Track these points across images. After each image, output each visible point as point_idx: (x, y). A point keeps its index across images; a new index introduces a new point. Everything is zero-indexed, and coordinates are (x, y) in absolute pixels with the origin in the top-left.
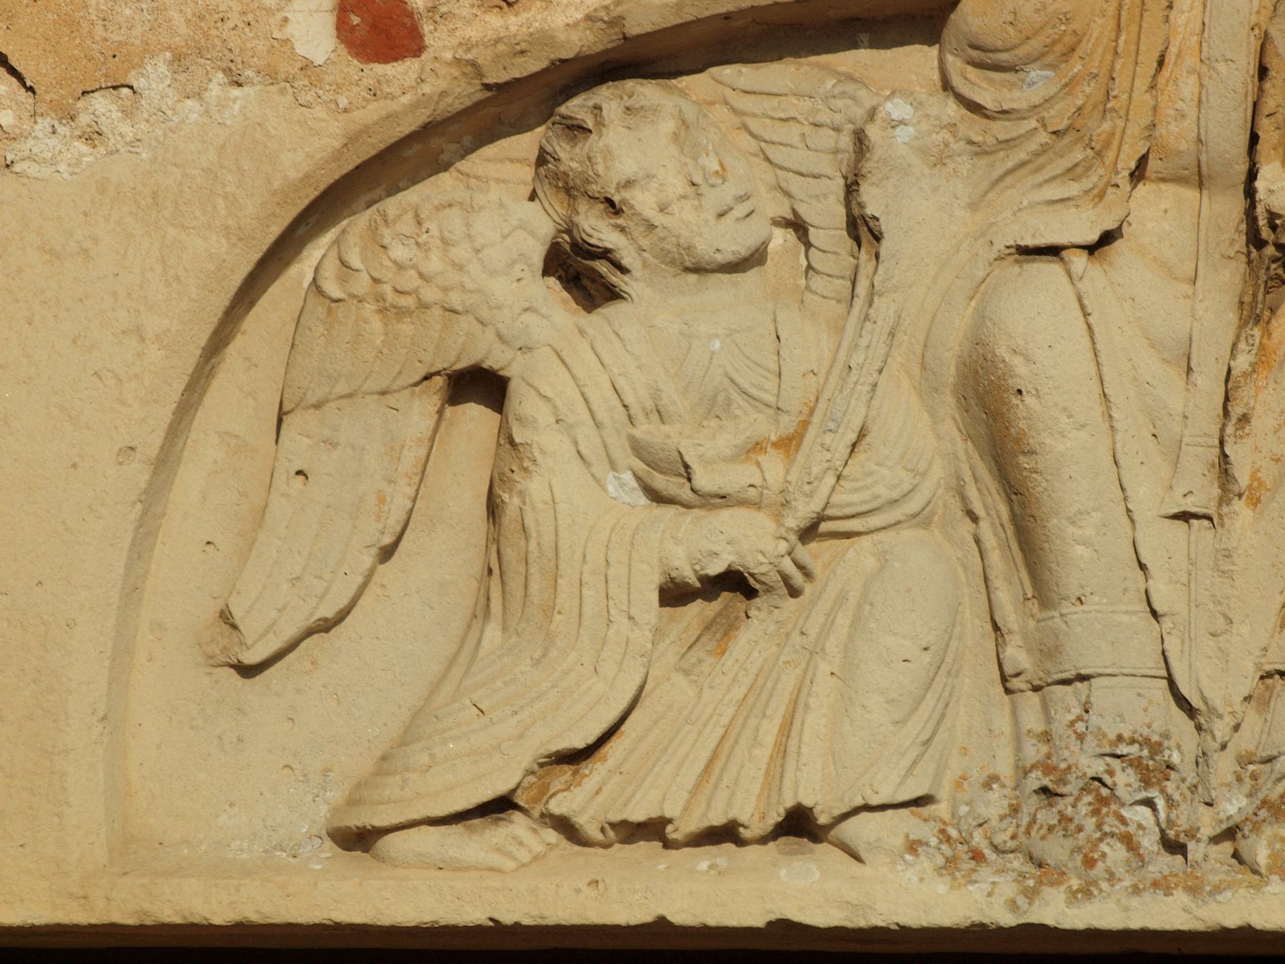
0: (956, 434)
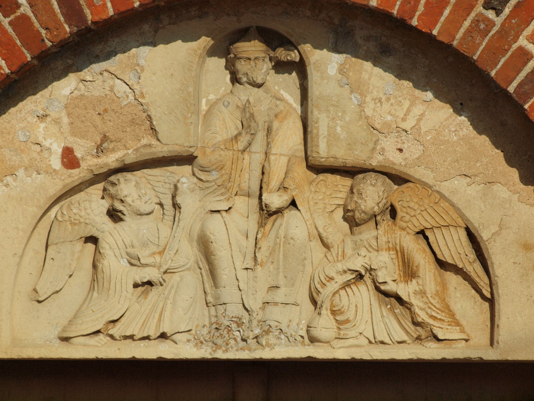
0: (197, 250)
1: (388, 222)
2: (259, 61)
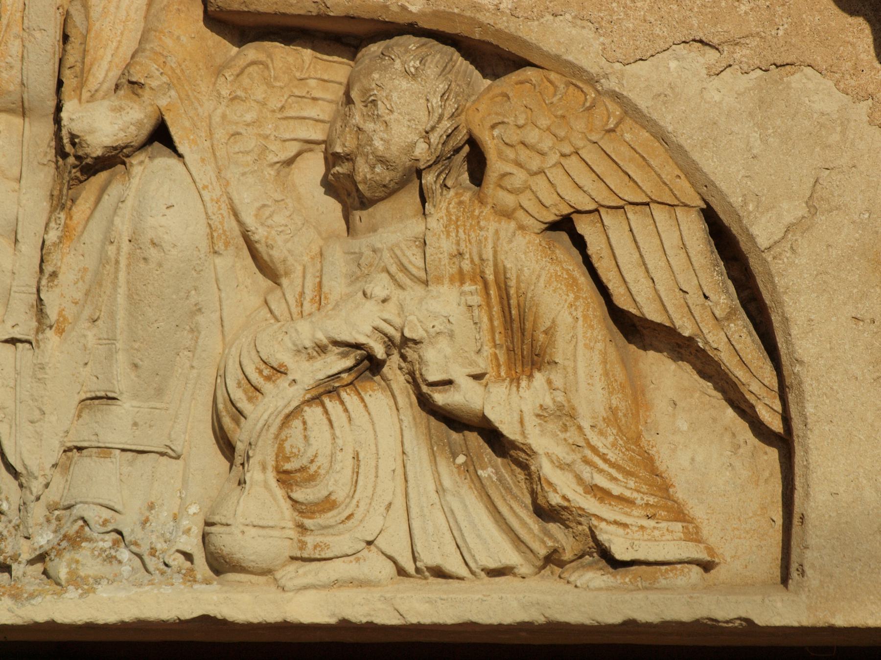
1: (462, 195)
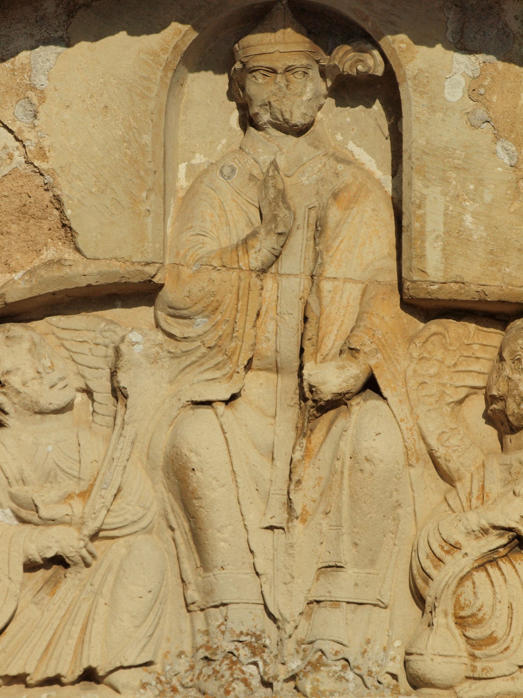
0: (163, 489)
2: (296, 75)
